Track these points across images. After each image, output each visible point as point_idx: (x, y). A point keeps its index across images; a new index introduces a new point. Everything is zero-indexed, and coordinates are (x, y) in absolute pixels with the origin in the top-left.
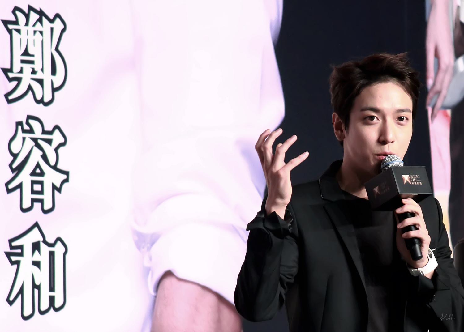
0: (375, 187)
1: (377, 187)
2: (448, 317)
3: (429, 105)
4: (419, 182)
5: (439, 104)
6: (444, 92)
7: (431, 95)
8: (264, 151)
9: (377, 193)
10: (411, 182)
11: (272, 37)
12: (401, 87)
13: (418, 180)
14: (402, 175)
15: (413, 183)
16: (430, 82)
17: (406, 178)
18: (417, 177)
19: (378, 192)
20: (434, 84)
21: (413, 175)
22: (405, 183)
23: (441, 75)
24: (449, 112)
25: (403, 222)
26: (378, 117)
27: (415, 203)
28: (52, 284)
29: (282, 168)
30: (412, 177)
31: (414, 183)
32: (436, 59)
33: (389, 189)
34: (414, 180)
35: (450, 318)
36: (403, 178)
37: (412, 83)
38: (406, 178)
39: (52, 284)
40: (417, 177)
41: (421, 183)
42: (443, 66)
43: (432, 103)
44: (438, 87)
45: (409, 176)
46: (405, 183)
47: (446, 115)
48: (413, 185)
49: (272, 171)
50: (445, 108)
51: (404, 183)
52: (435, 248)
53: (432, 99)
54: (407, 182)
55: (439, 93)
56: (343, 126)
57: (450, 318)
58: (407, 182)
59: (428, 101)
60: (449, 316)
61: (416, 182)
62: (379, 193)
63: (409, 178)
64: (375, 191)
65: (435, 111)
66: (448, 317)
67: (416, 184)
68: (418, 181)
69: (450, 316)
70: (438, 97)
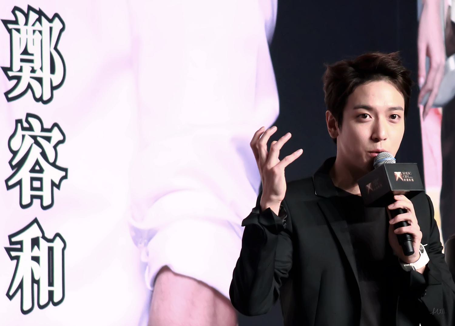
0: (368, 184)
1: (370, 184)
2: (439, 311)
3: (421, 103)
4: (411, 179)
5: (430, 103)
6: (435, 91)
7: (422, 93)
8: (259, 148)
9: (370, 190)
10: (403, 178)
11: (267, 37)
12: (393, 85)
13: (410, 176)
14: (395, 172)
15: (405, 180)
16: (422, 81)
17: (398, 174)
18: (409, 173)
19: (371, 188)
20: (426, 83)
21: (405, 171)
22: (397, 180)
23: (432, 74)
24: (440, 110)
25: (395, 218)
26: (371, 115)
27: (407, 199)
28: (51, 279)
29: (276, 165)
30: (404, 173)
31: (406, 180)
32: (428, 58)
33: (381, 185)
34: (406, 176)
35: (442, 312)
36: (395, 174)
37: (404, 82)
38: (398, 174)
39: (51, 279)
40: (409, 173)
41: (413, 180)
42: (434, 65)
43: (424, 101)
44: (429, 85)
45: (401, 172)
46: (397, 180)
47: (437, 113)
48: (405, 181)
49: (266, 168)
50: (436, 106)
51: (396, 180)
52: (426, 244)
53: (423, 97)
54: (399, 179)
55: (430, 91)
56: (336, 124)
57: (442, 312)
58: (399, 179)
59: (420, 99)
60: (440, 310)
61: (408, 179)
62: (372, 190)
63: (401, 174)
64: (368, 188)
65: (427, 109)
66: (439, 311)
67: (408, 180)
68: (410, 177)
69: (442, 310)
70: (430, 95)
